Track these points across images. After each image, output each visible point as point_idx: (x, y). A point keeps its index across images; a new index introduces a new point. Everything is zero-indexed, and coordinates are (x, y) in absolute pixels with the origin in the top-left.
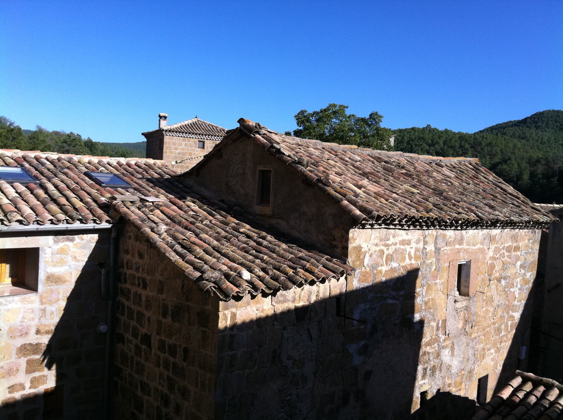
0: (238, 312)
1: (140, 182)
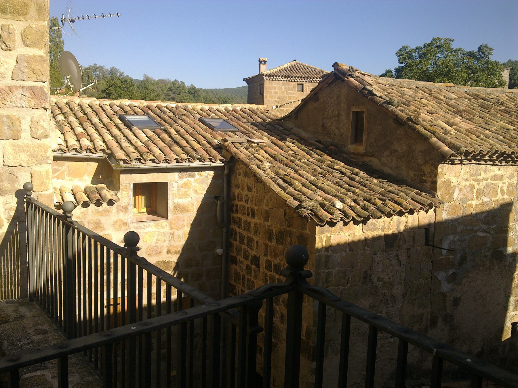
0: (332, 236)
1: (245, 125)
